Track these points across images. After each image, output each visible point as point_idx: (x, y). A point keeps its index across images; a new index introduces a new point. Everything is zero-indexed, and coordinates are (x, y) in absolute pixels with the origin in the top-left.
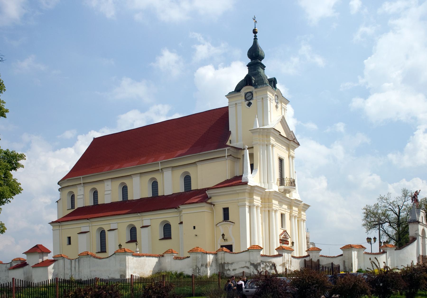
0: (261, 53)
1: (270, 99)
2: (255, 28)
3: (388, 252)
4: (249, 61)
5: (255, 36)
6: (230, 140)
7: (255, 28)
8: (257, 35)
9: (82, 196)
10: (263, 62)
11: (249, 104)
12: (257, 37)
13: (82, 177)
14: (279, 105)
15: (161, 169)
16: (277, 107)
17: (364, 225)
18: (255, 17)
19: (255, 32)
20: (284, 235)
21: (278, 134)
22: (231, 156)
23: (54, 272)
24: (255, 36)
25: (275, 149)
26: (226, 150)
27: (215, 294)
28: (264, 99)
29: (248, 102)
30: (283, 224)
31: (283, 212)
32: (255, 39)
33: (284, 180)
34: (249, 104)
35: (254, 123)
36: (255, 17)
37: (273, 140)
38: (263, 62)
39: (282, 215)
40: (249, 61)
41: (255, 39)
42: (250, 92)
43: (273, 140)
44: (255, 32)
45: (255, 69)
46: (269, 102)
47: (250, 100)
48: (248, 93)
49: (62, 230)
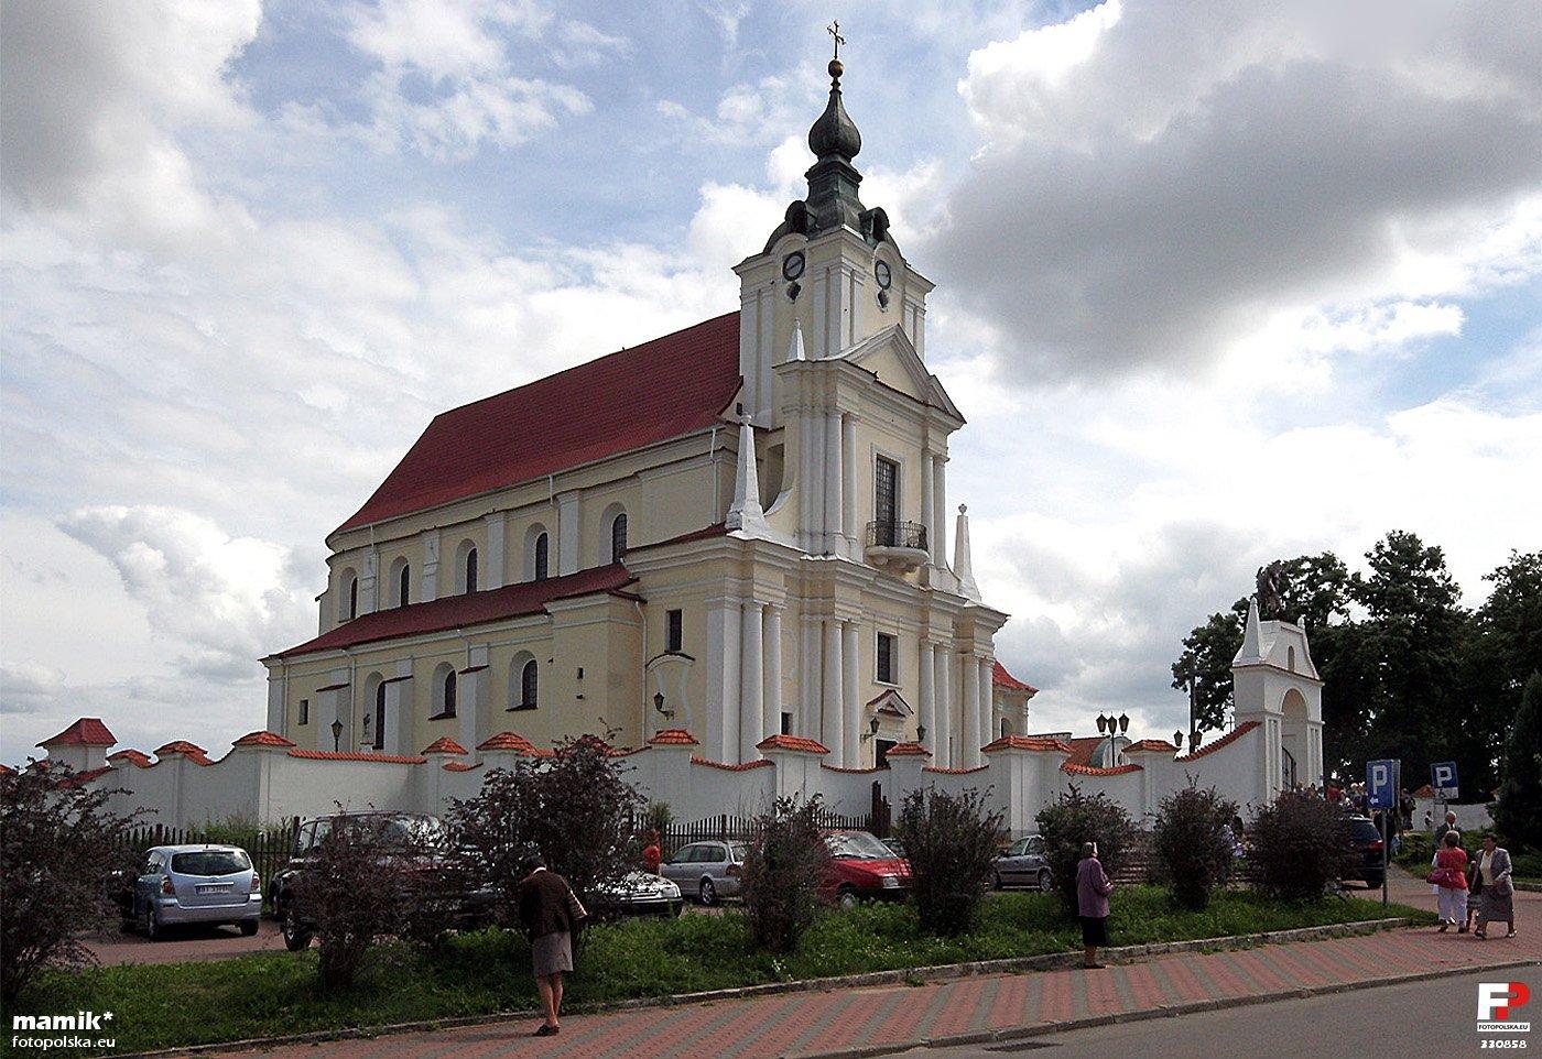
0: (845, 136)
1: (853, 272)
2: (836, 57)
3: (1147, 769)
4: (813, 160)
5: (836, 84)
6: (739, 405)
7: (836, 57)
8: (839, 79)
9: (371, 582)
10: (855, 162)
11: (794, 292)
12: (840, 88)
13: (374, 527)
14: (893, 296)
15: (554, 497)
16: (882, 299)
17: (276, 578)
18: (837, 26)
19: (835, 69)
20: (889, 704)
21: (869, 381)
22: (724, 451)
23: (1492, 864)
24: (836, 84)
25: (855, 430)
26: (712, 432)
27: (358, 862)
28: (832, 273)
29: (790, 283)
30: (885, 671)
31: (892, 632)
32: (835, 92)
33: (899, 528)
34: (794, 292)
35: (790, 344)
36: (837, 26)
37: (846, 399)
38: (855, 162)
39: (885, 640)
40: (813, 160)
41: (835, 92)
42: (796, 253)
43: (846, 399)
44: (835, 69)
45: (826, 185)
46: (846, 282)
47: (798, 276)
48: (792, 255)
49: (281, 669)
